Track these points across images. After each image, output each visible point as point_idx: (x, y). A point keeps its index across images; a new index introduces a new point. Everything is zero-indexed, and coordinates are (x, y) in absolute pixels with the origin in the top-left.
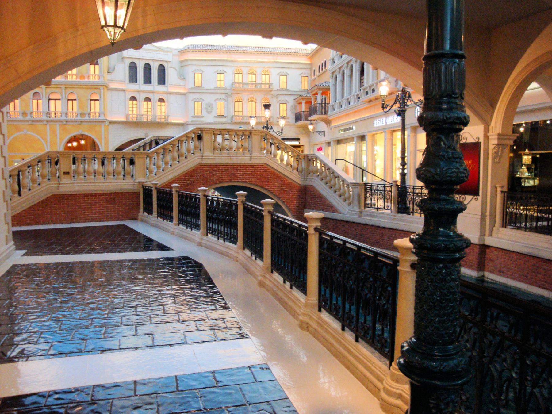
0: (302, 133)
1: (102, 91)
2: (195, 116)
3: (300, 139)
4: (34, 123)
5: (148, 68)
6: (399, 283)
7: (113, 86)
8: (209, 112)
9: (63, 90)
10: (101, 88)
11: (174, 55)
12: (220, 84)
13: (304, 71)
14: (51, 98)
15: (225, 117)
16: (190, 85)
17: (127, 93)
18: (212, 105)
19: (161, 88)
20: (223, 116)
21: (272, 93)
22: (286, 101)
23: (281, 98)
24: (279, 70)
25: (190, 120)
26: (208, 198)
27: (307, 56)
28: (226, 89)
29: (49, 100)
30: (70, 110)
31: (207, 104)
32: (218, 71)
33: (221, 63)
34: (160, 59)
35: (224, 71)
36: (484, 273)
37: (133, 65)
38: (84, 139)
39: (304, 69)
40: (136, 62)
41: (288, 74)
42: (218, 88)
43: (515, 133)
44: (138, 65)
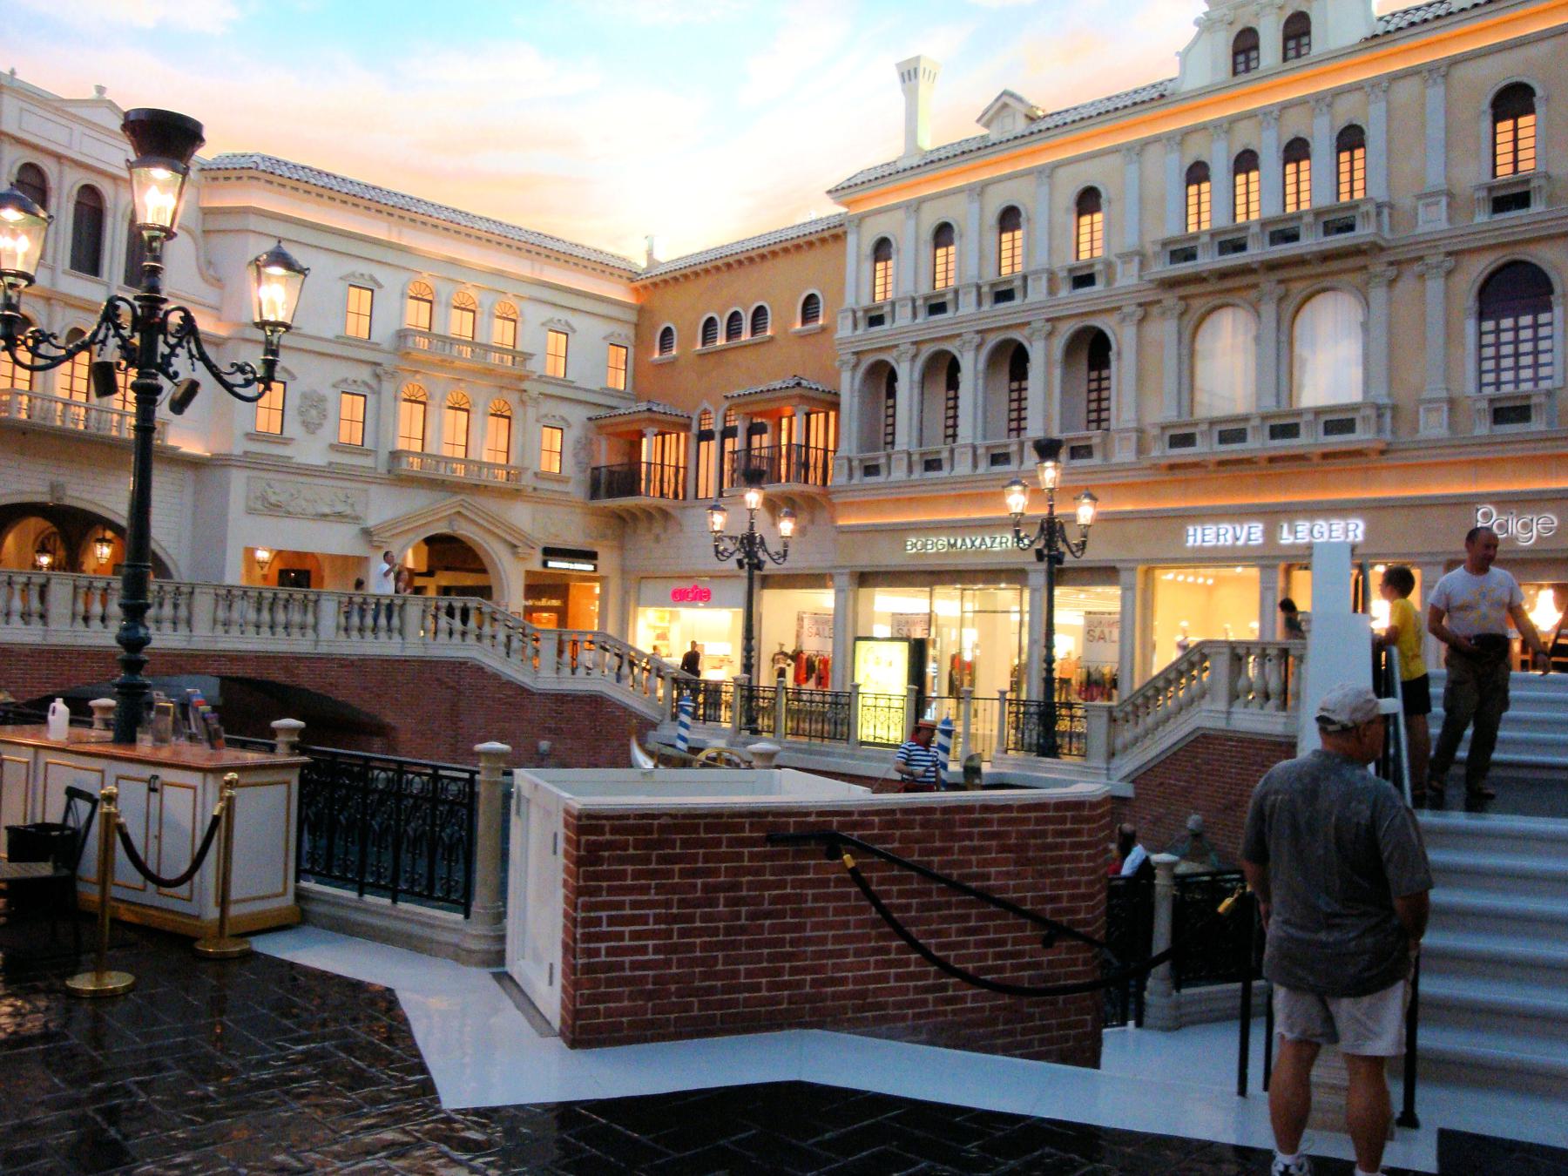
0: (604, 537)
2: (252, 436)
3: (599, 557)
8: (311, 427)
12: (357, 327)
15: (367, 453)
18: (323, 399)
20: (360, 450)
21: (526, 385)
22: (563, 419)
23: (549, 407)
24: (548, 313)
25: (238, 447)
27: (631, 280)
28: (375, 347)
31: (304, 396)
32: (353, 275)
33: (367, 250)
34: (43, 144)
35: (373, 279)
36: (1261, 1015)
37: (31, 178)
38: (537, 748)
39: (619, 320)
40: (49, 167)
42: (343, 340)
44: (109, 204)
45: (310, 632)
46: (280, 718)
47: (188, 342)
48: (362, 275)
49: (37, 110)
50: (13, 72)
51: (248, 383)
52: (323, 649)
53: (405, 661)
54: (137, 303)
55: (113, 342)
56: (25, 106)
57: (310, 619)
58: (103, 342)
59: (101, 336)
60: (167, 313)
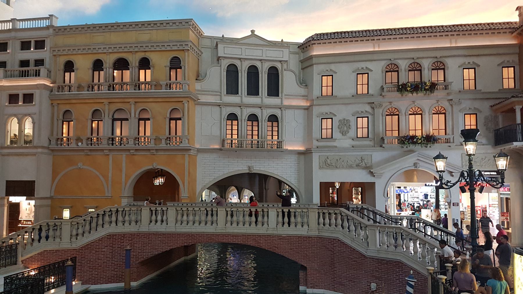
1: (186, 105)
4: (94, 153)
5: (253, 72)
6: (114, 61)
7: (203, 99)
9: (133, 106)
10: (185, 101)
11: (291, 53)
13: (506, 58)
14: (115, 117)
16: (316, 93)
17: (224, 109)
19: (274, 101)
24: (461, 60)
26: (305, 85)
29: (114, 120)
30: (142, 134)
41: (478, 66)
43: (268, 202)
45: (265, 225)
46: (151, 279)
47: (481, 177)
48: (363, 68)
49: (229, 46)
50: (223, 36)
51: (497, 184)
52: (270, 232)
53: (308, 238)
54: (468, 171)
55: (463, 181)
56: (225, 46)
57: (305, 220)
58: (461, 181)
59: (460, 180)
60: (475, 172)
